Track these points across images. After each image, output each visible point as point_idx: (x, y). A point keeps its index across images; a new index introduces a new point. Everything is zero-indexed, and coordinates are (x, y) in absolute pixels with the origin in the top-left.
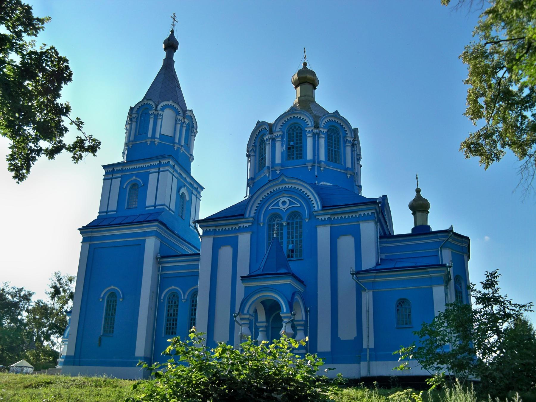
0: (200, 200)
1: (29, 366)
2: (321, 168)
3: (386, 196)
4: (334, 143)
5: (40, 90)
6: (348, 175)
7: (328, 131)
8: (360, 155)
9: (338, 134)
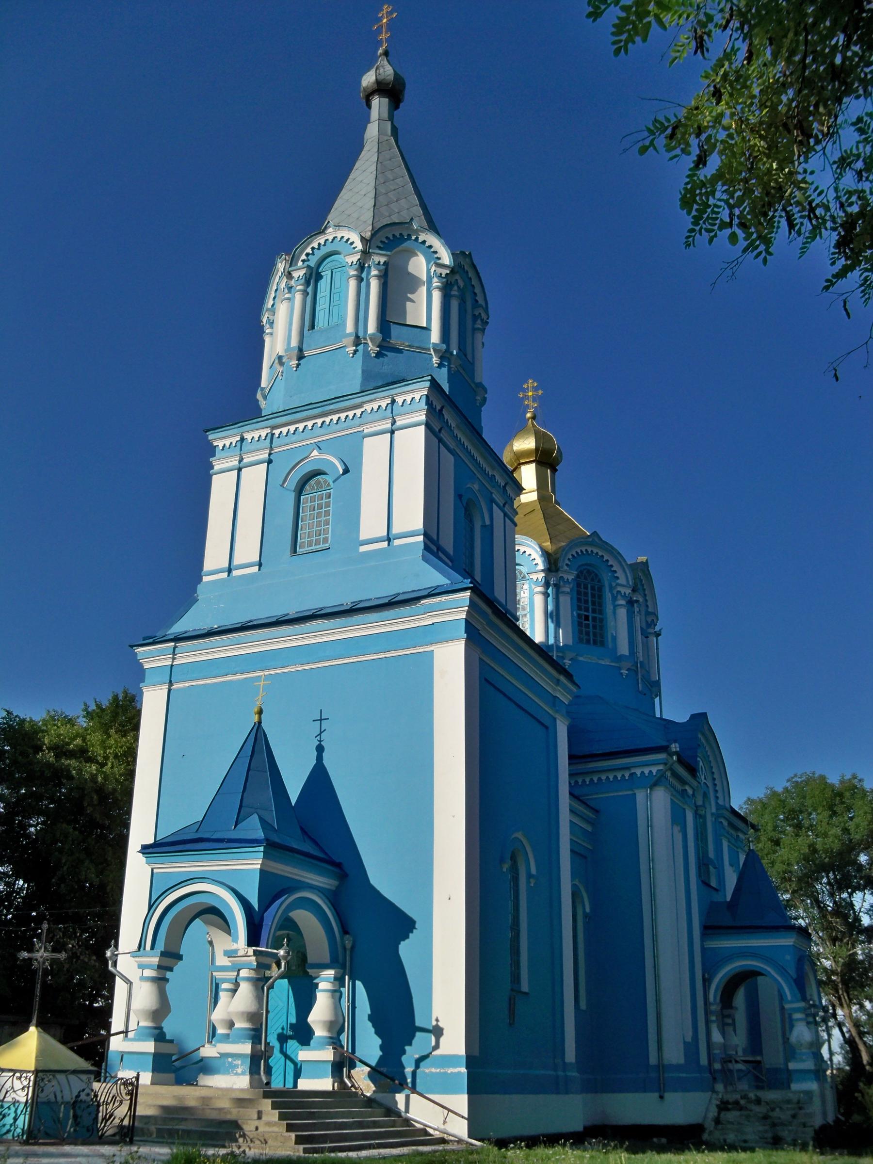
0: (516, 525)
1: (71, 1067)
2: (564, 659)
3: (704, 716)
4: (592, 601)
5: (31, 949)
6: (622, 671)
7: (578, 576)
8: (655, 615)
9: (599, 581)
